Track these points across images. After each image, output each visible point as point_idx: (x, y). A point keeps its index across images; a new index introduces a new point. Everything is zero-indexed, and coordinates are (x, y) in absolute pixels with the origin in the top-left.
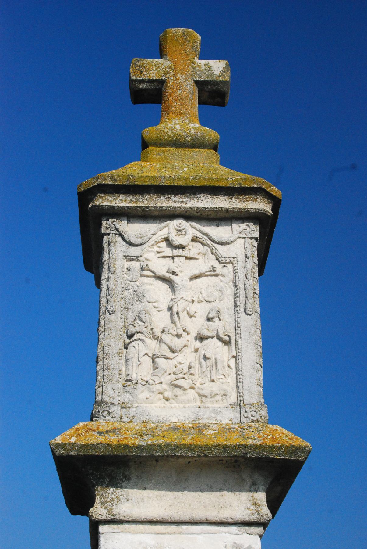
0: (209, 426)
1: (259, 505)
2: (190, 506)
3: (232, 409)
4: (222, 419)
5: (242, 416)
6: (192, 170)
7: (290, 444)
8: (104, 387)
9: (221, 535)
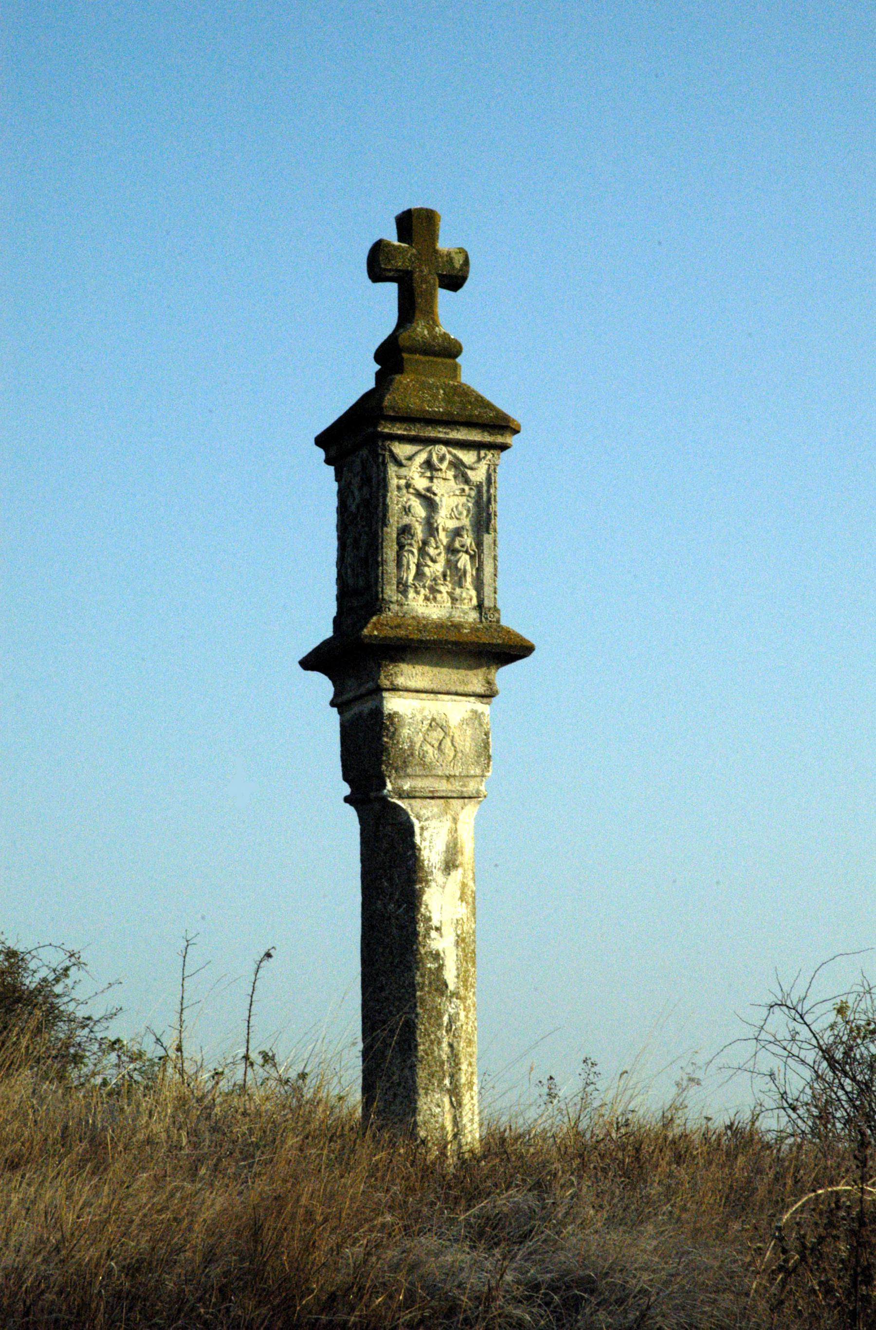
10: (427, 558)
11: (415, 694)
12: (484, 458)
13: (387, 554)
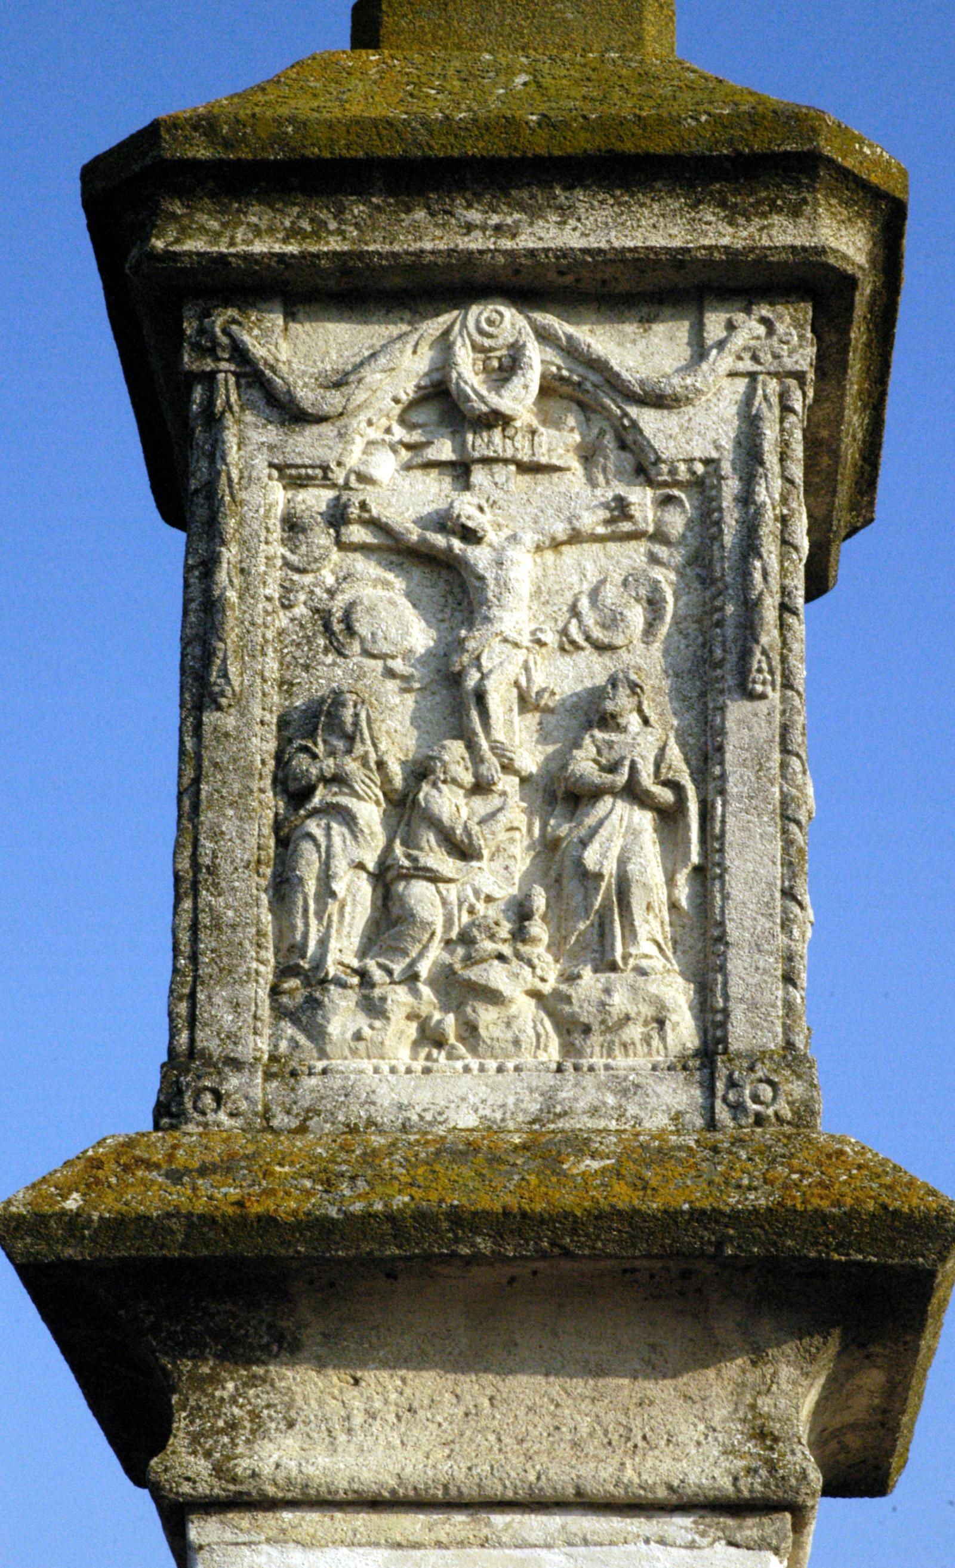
0: (587, 1141)
1: (776, 1440)
2: (521, 1442)
3: (682, 1075)
4: (642, 1114)
5: (719, 1104)
6: (547, 81)
7: (884, 1207)
8: (201, 996)
9: (631, 1548)
10: (429, 838)
11: (362, 1521)
12: (721, 345)
13: (217, 835)
